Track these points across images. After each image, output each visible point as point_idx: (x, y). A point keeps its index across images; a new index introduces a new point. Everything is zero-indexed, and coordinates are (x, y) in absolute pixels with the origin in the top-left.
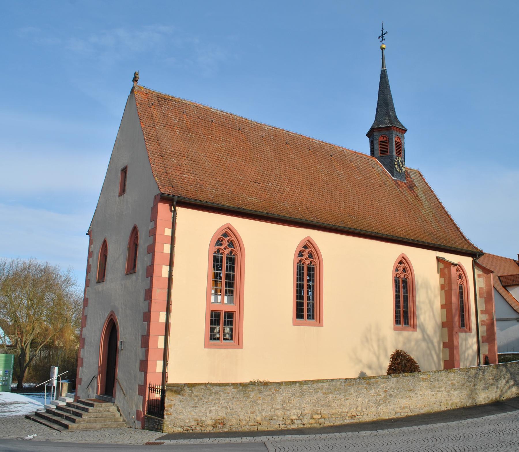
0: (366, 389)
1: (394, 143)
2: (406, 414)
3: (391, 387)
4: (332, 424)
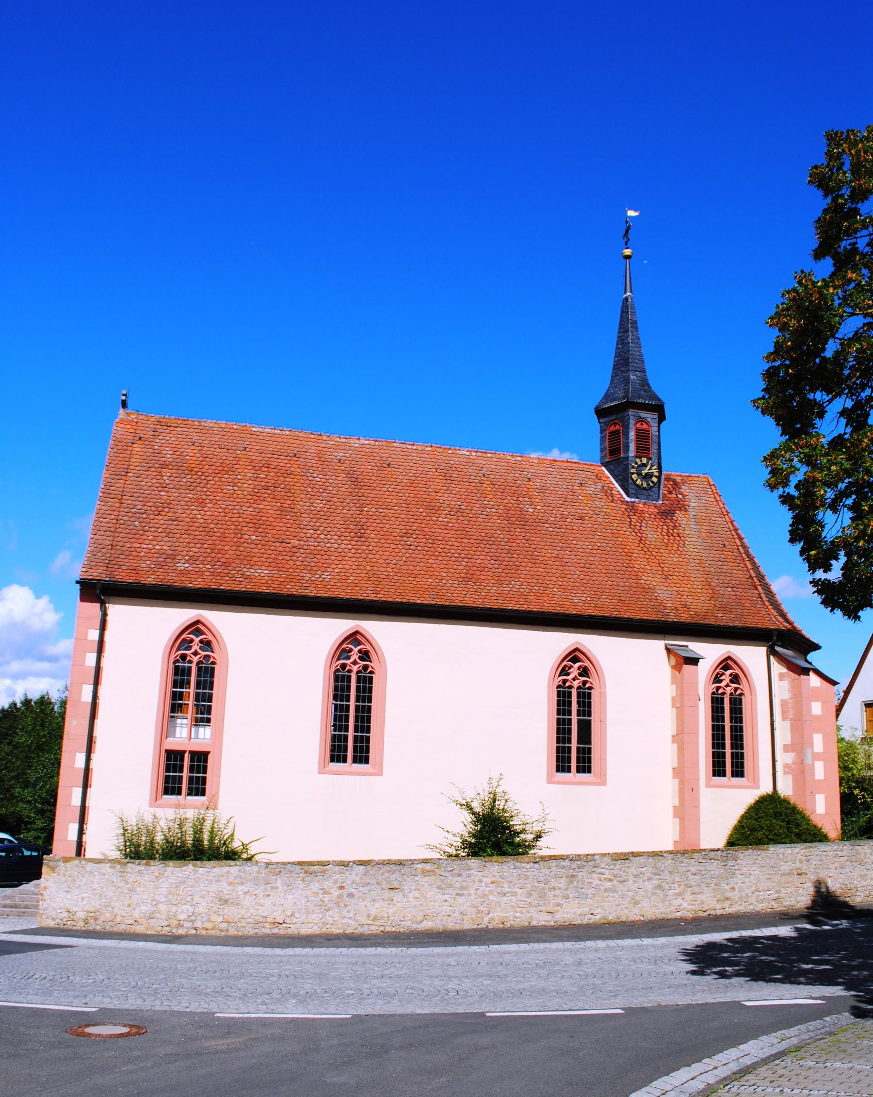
0: (303, 880)
1: (632, 434)
2: (382, 929)
3: (353, 882)
4: (240, 933)
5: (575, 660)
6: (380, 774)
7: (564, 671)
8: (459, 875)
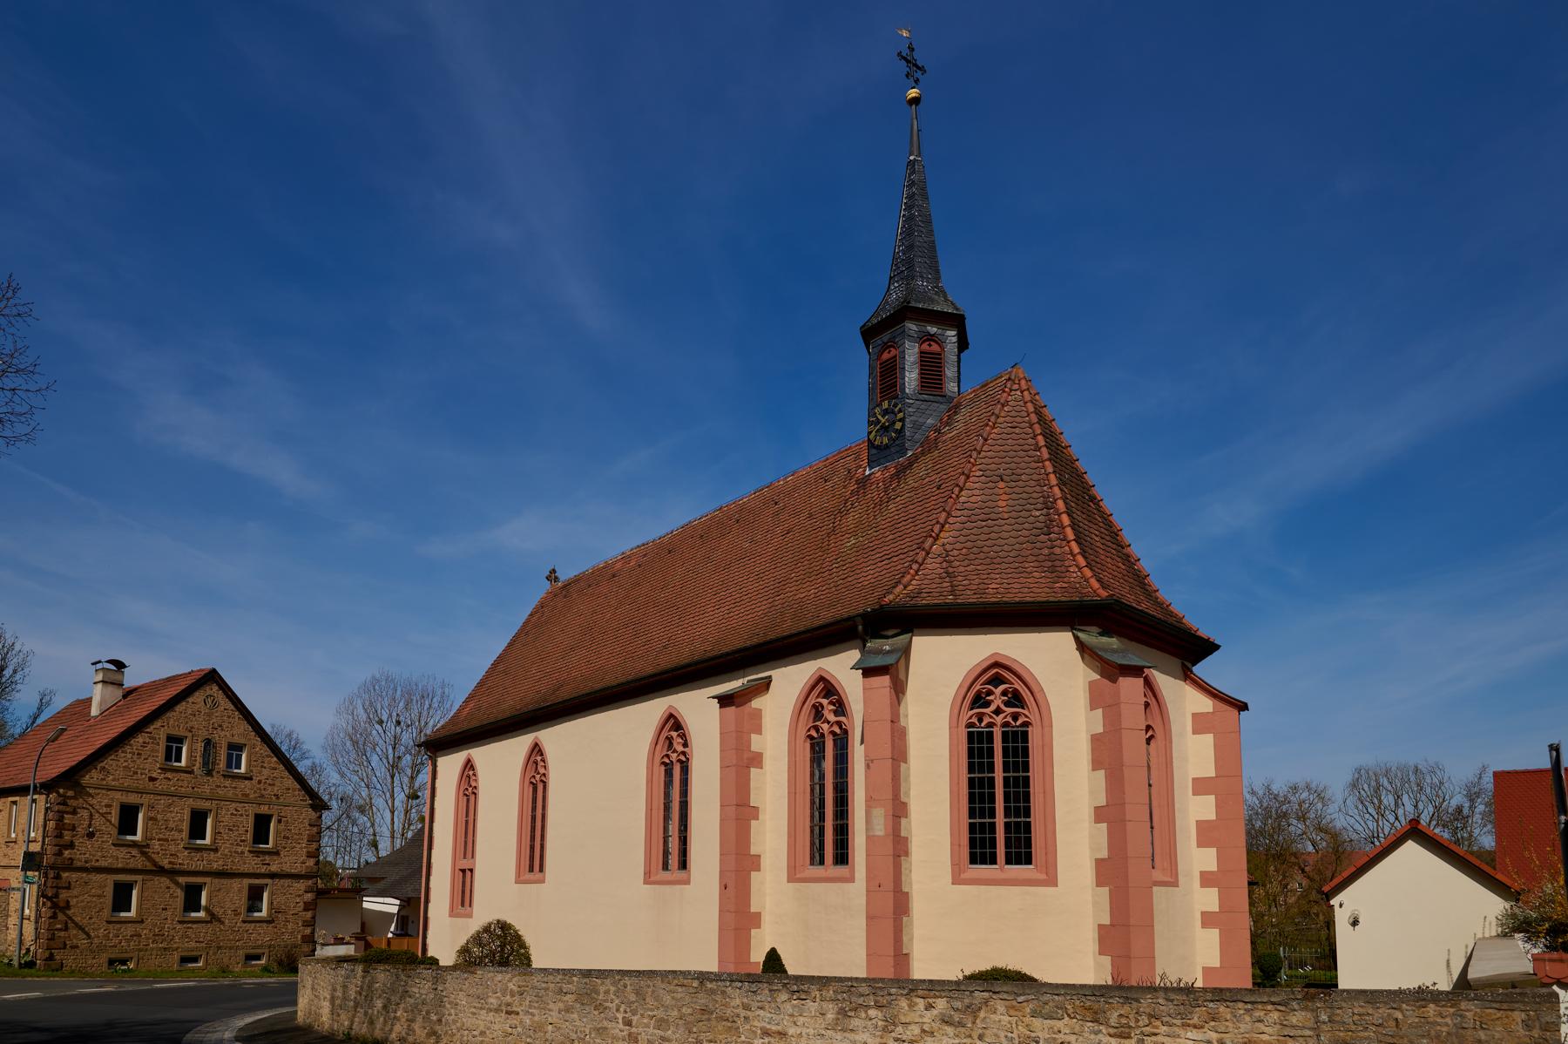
5: (997, 680)
6: (1052, 881)
7: (980, 701)
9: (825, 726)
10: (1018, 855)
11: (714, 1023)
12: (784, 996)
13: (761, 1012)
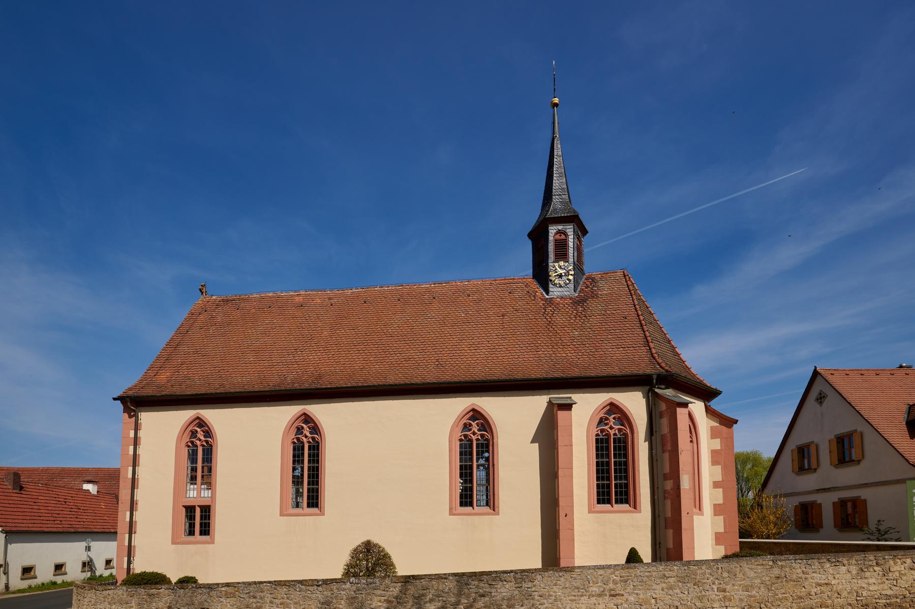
1: (571, 260)
7: (467, 427)
8: (255, 597)
9: (198, 442)
10: (466, 502)
11: (784, 583)
12: (828, 565)
13: (814, 575)
